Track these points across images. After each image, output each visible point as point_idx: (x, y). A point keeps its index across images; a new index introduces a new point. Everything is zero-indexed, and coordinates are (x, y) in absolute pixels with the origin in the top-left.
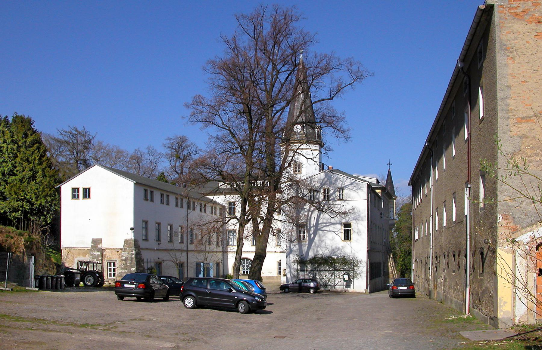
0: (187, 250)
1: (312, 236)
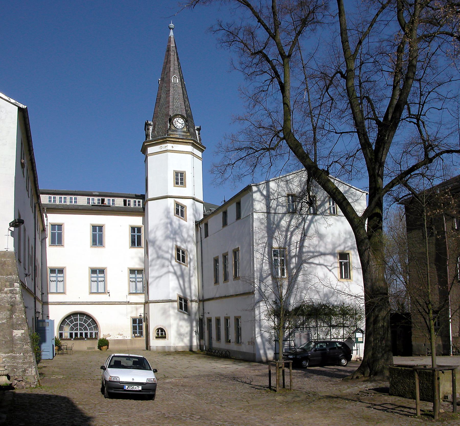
1: (295, 271)
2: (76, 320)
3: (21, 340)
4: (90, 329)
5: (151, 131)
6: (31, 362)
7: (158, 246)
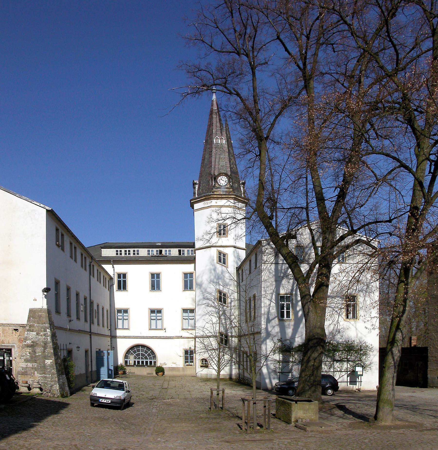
0: (90, 332)
2: (138, 351)
3: (50, 367)
4: (150, 358)
5: (196, 189)
6: (56, 381)
7: (204, 288)
